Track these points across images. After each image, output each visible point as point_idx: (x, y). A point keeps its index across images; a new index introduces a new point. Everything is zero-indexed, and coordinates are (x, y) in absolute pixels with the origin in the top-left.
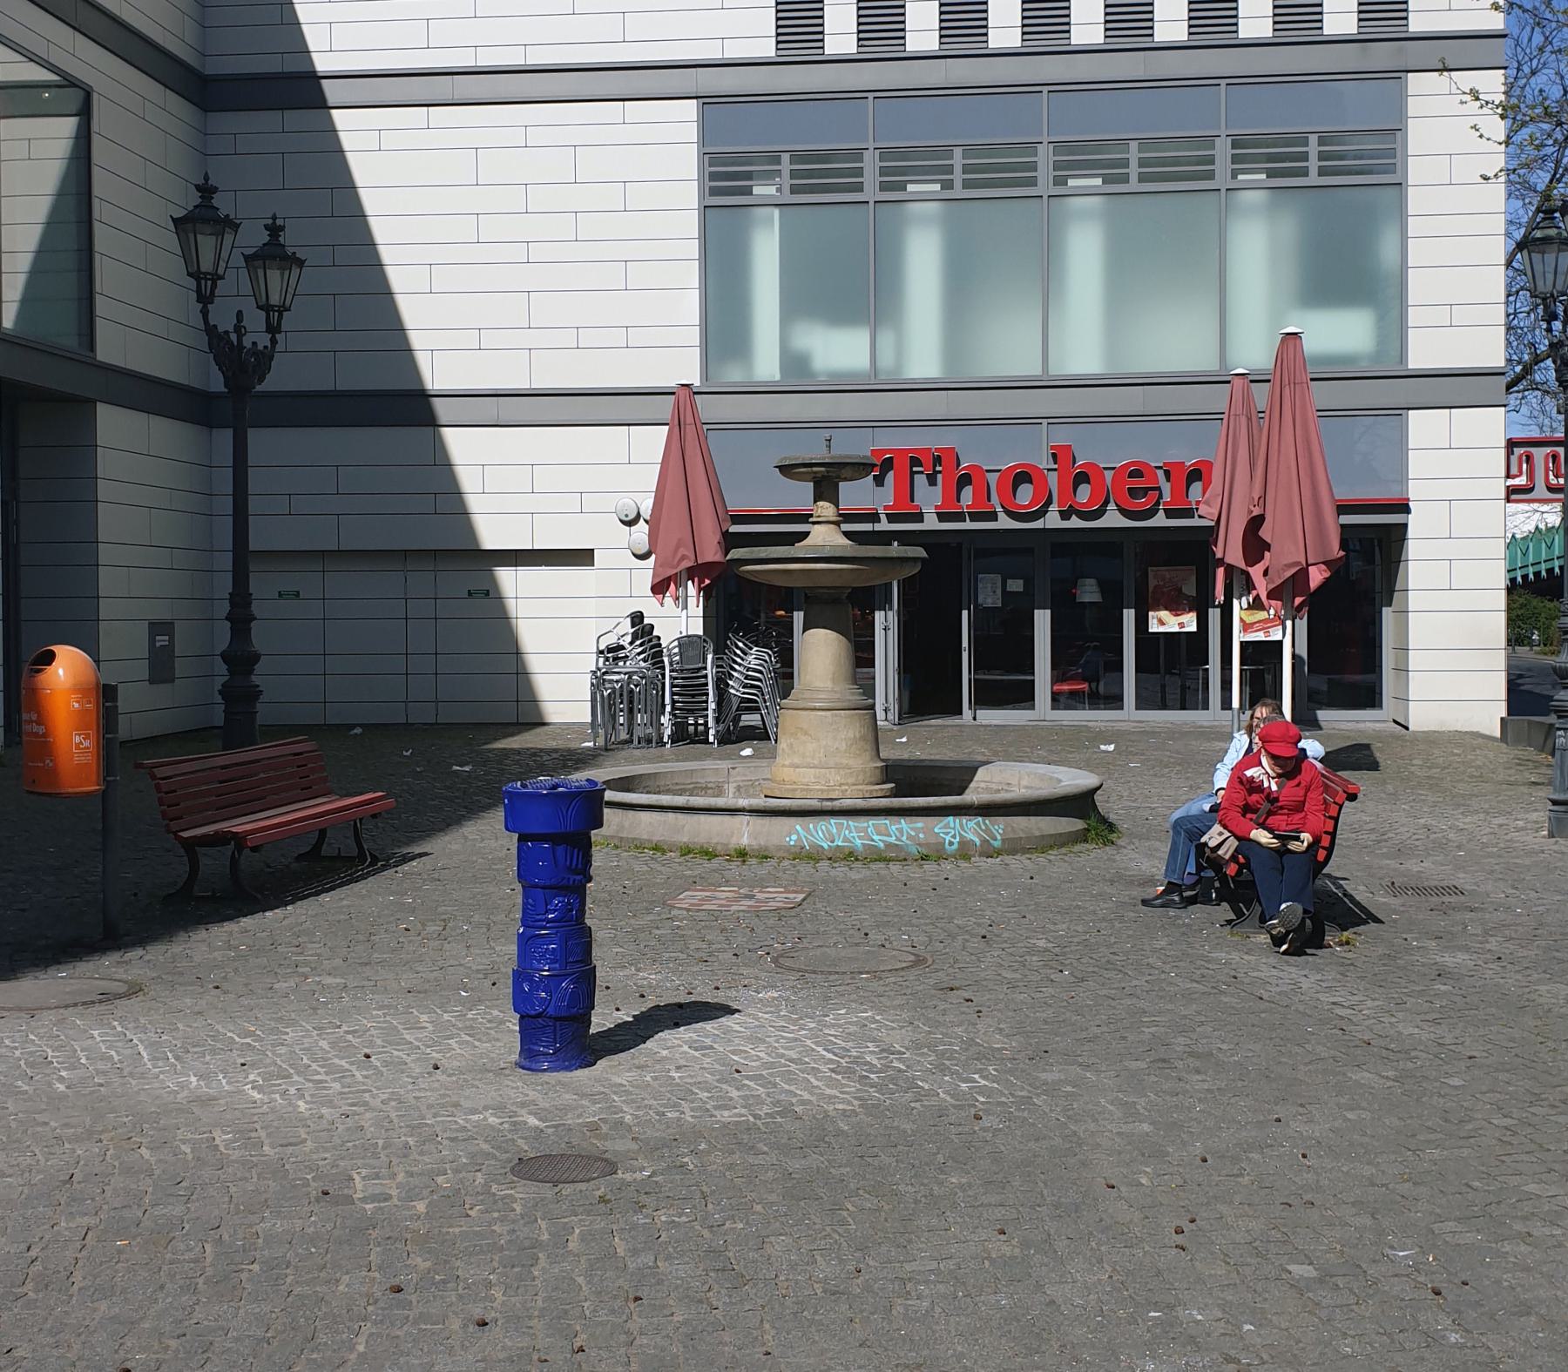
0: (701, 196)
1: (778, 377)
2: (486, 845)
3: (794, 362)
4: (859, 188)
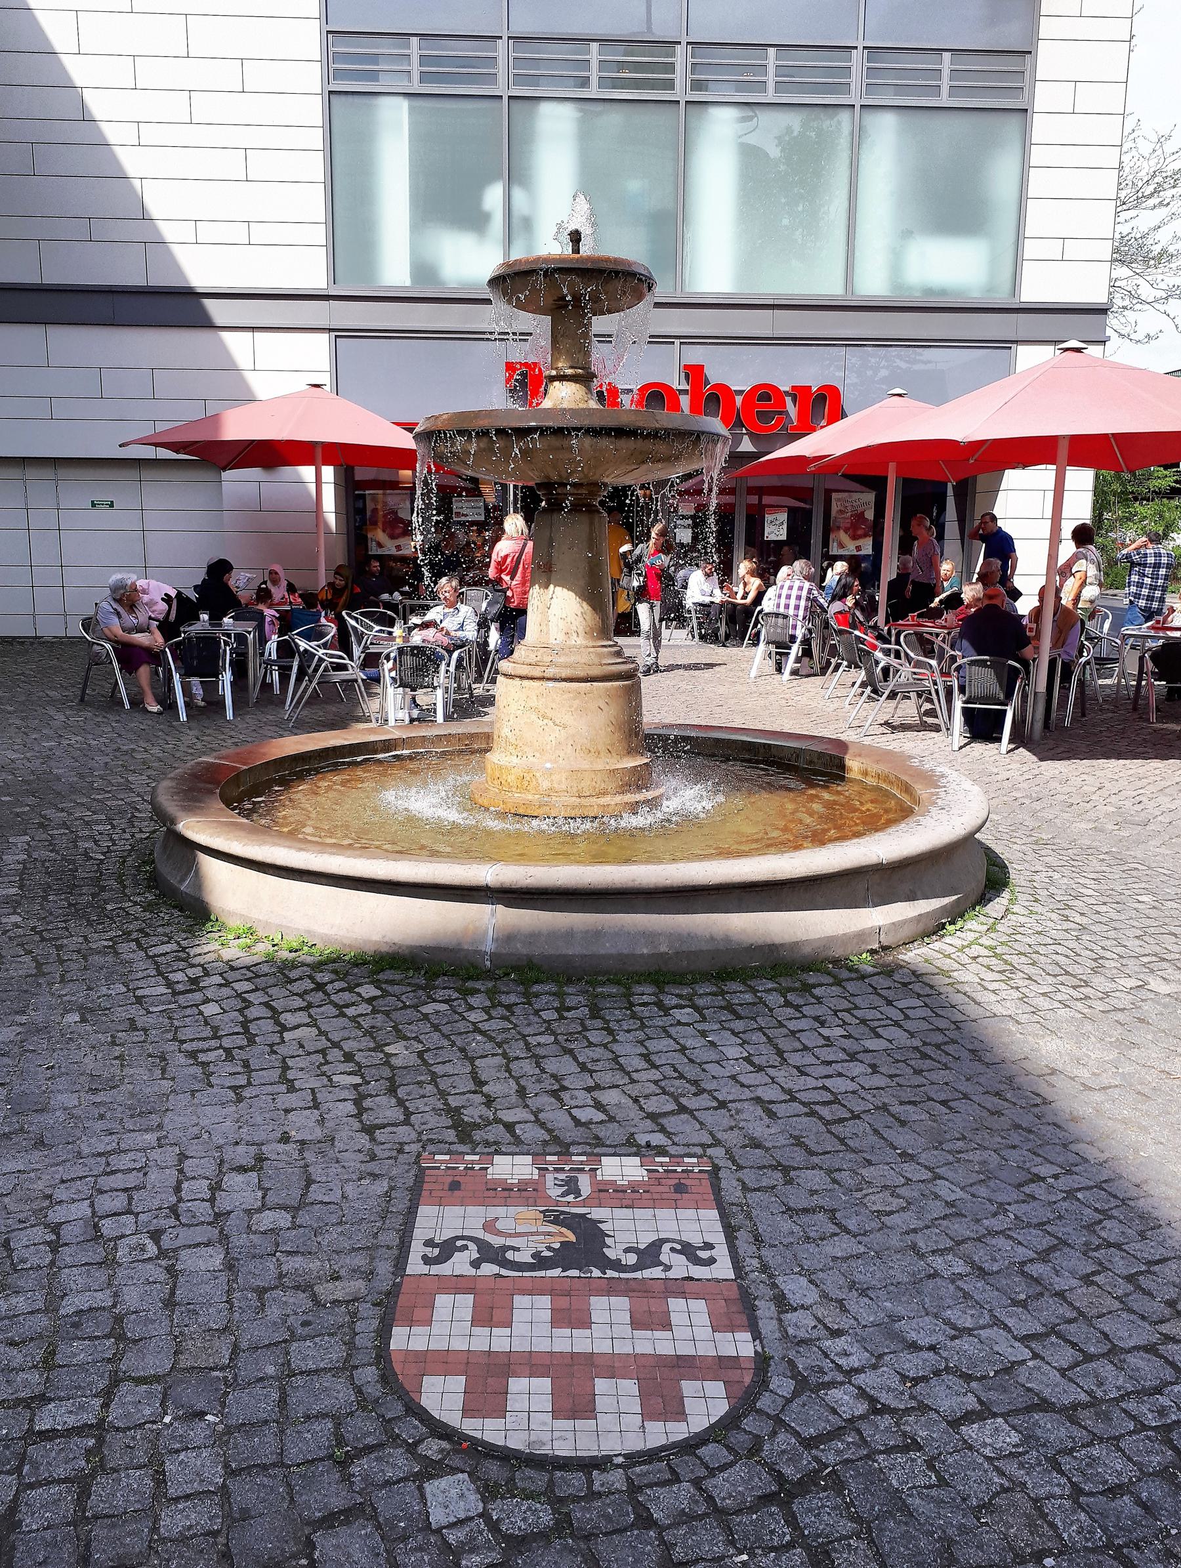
0: (327, 78)
1: (408, 283)
2: (1002, 696)
3: (423, 270)
4: (669, 85)
